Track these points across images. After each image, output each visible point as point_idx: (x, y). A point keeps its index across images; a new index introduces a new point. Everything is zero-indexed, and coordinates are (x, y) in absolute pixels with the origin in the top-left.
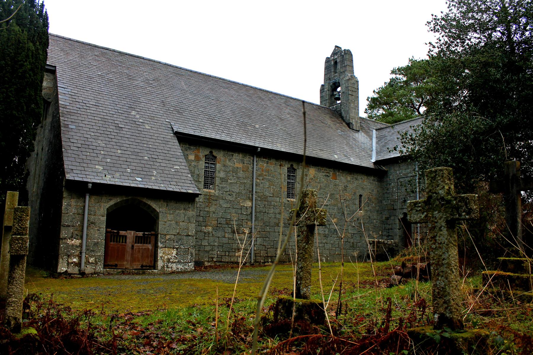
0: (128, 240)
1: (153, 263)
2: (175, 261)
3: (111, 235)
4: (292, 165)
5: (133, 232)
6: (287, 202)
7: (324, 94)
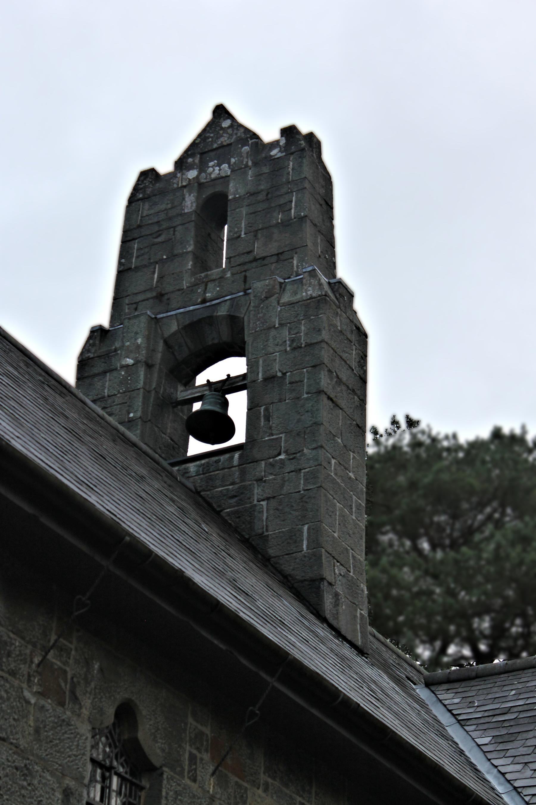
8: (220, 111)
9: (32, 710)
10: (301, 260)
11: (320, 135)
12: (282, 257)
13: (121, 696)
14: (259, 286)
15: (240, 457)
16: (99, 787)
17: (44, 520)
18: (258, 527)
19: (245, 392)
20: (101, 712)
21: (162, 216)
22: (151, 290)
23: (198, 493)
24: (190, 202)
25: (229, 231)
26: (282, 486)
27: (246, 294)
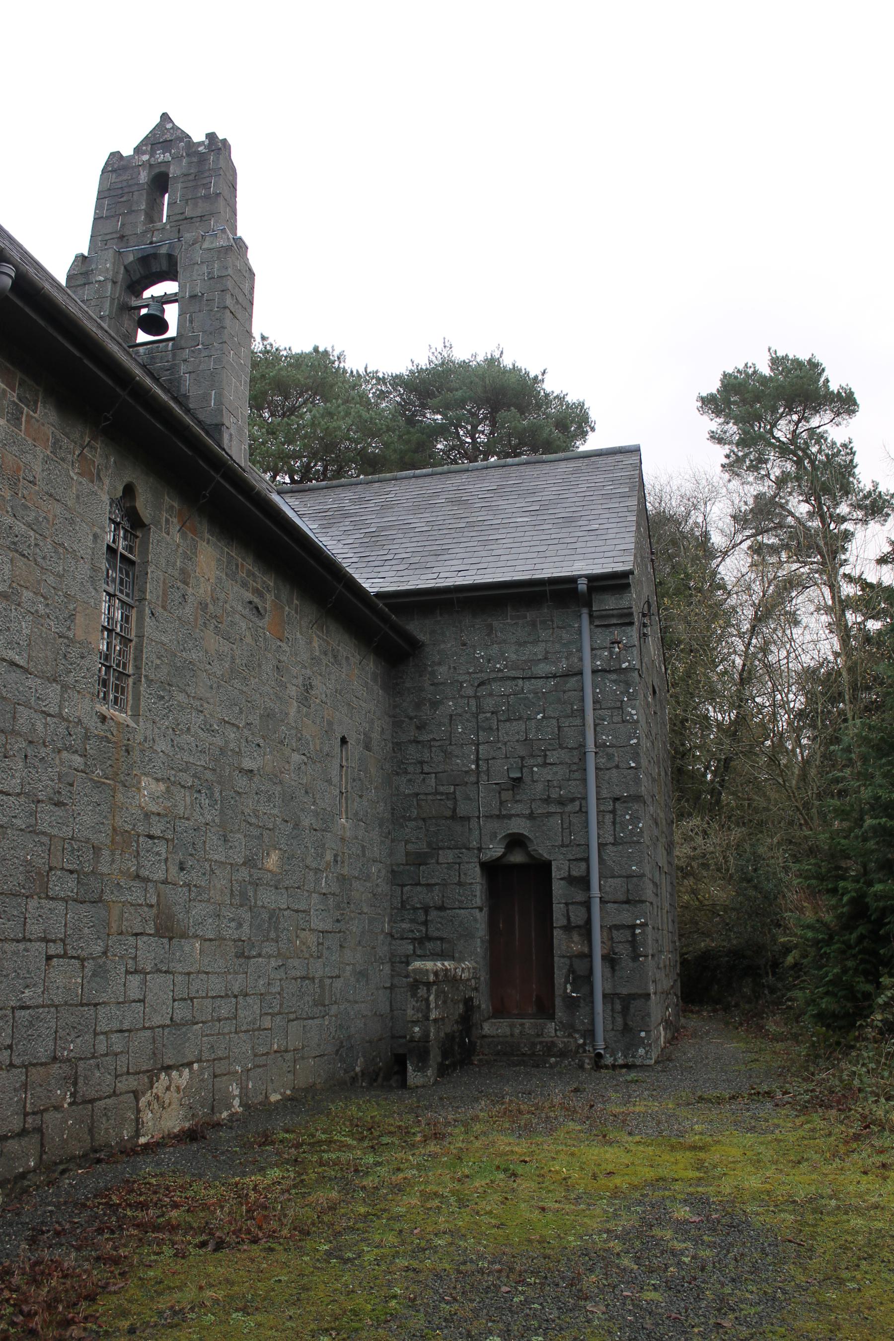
6: (93, 723)
8: (165, 117)
9: (74, 483)
10: (216, 222)
11: (231, 141)
12: (204, 219)
13: (127, 479)
14: (188, 236)
15: (173, 345)
16: (112, 534)
17: (86, 361)
18: (183, 391)
19: (176, 305)
20: (115, 488)
21: (125, 184)
22: (116, 232)
23: (145, 366)
24: (144, 177)
25: (169, 198)
26: (199, 366)
27: (179, 240)
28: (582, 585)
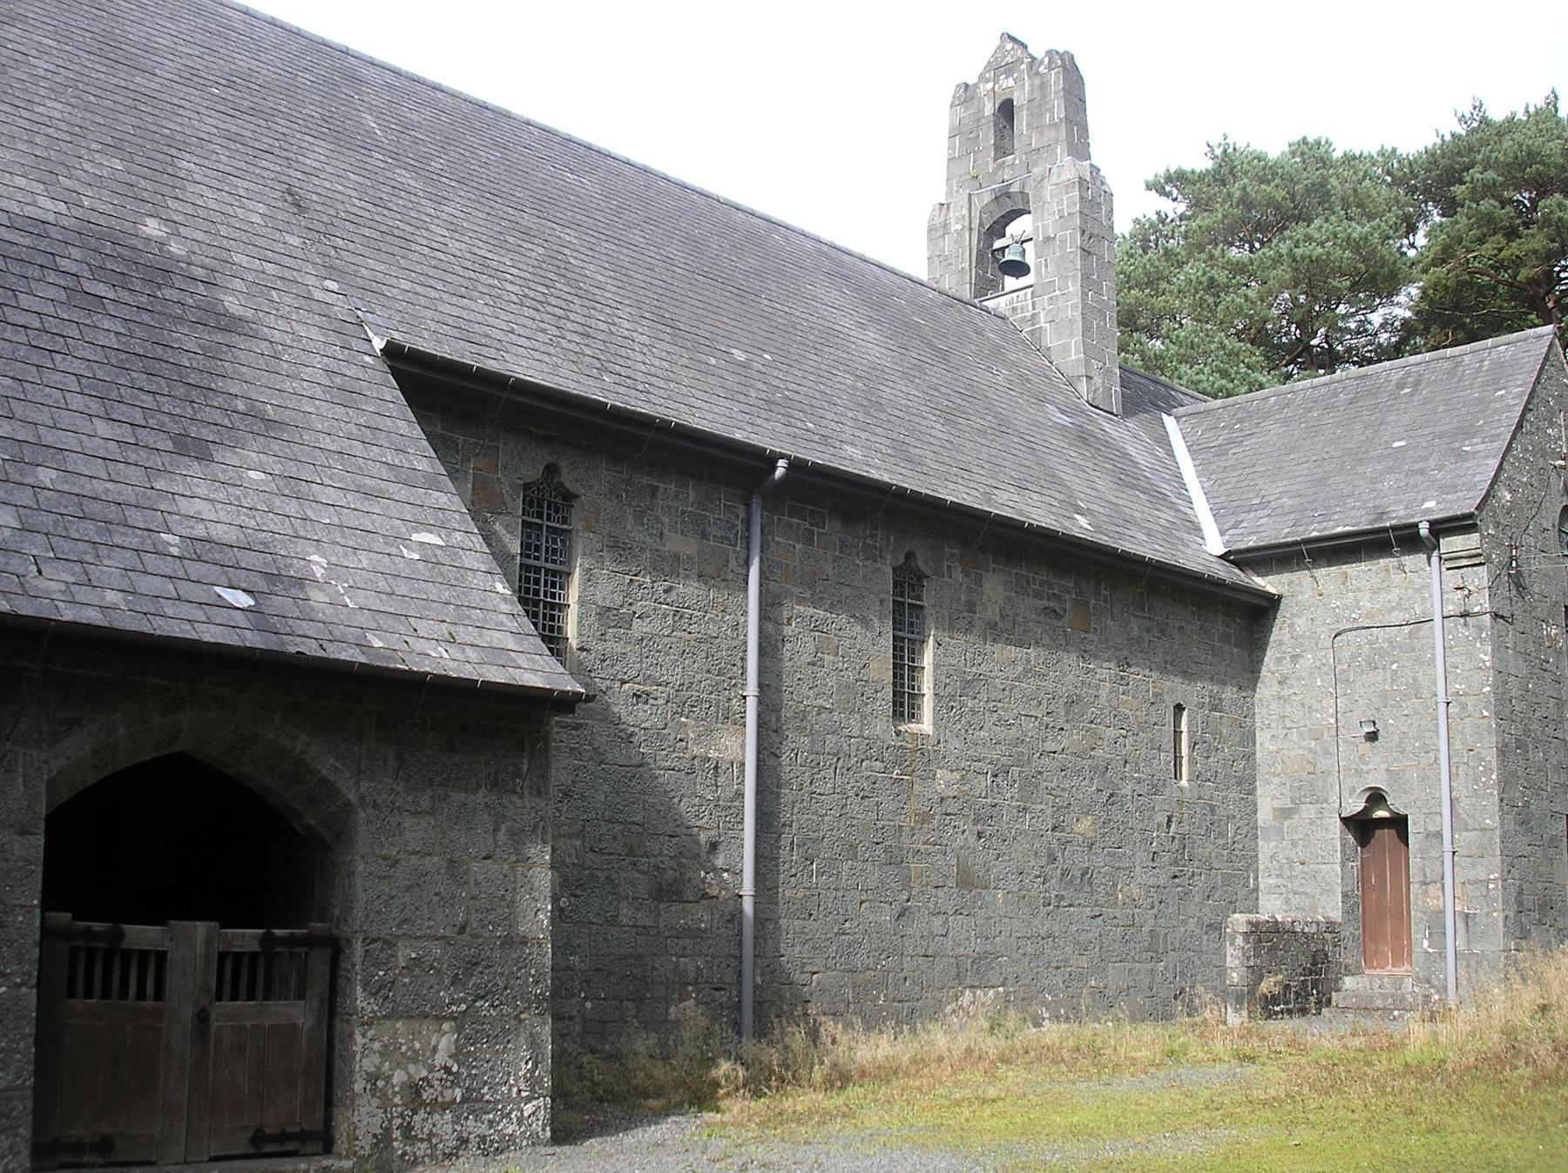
0: (173, 984)
1: (320, 1114)
2: (448, 1095)
3: (74, 952)
4: (910, 556)
5: (201, 929)
7: (948, 246)
28: (1424, 530)
